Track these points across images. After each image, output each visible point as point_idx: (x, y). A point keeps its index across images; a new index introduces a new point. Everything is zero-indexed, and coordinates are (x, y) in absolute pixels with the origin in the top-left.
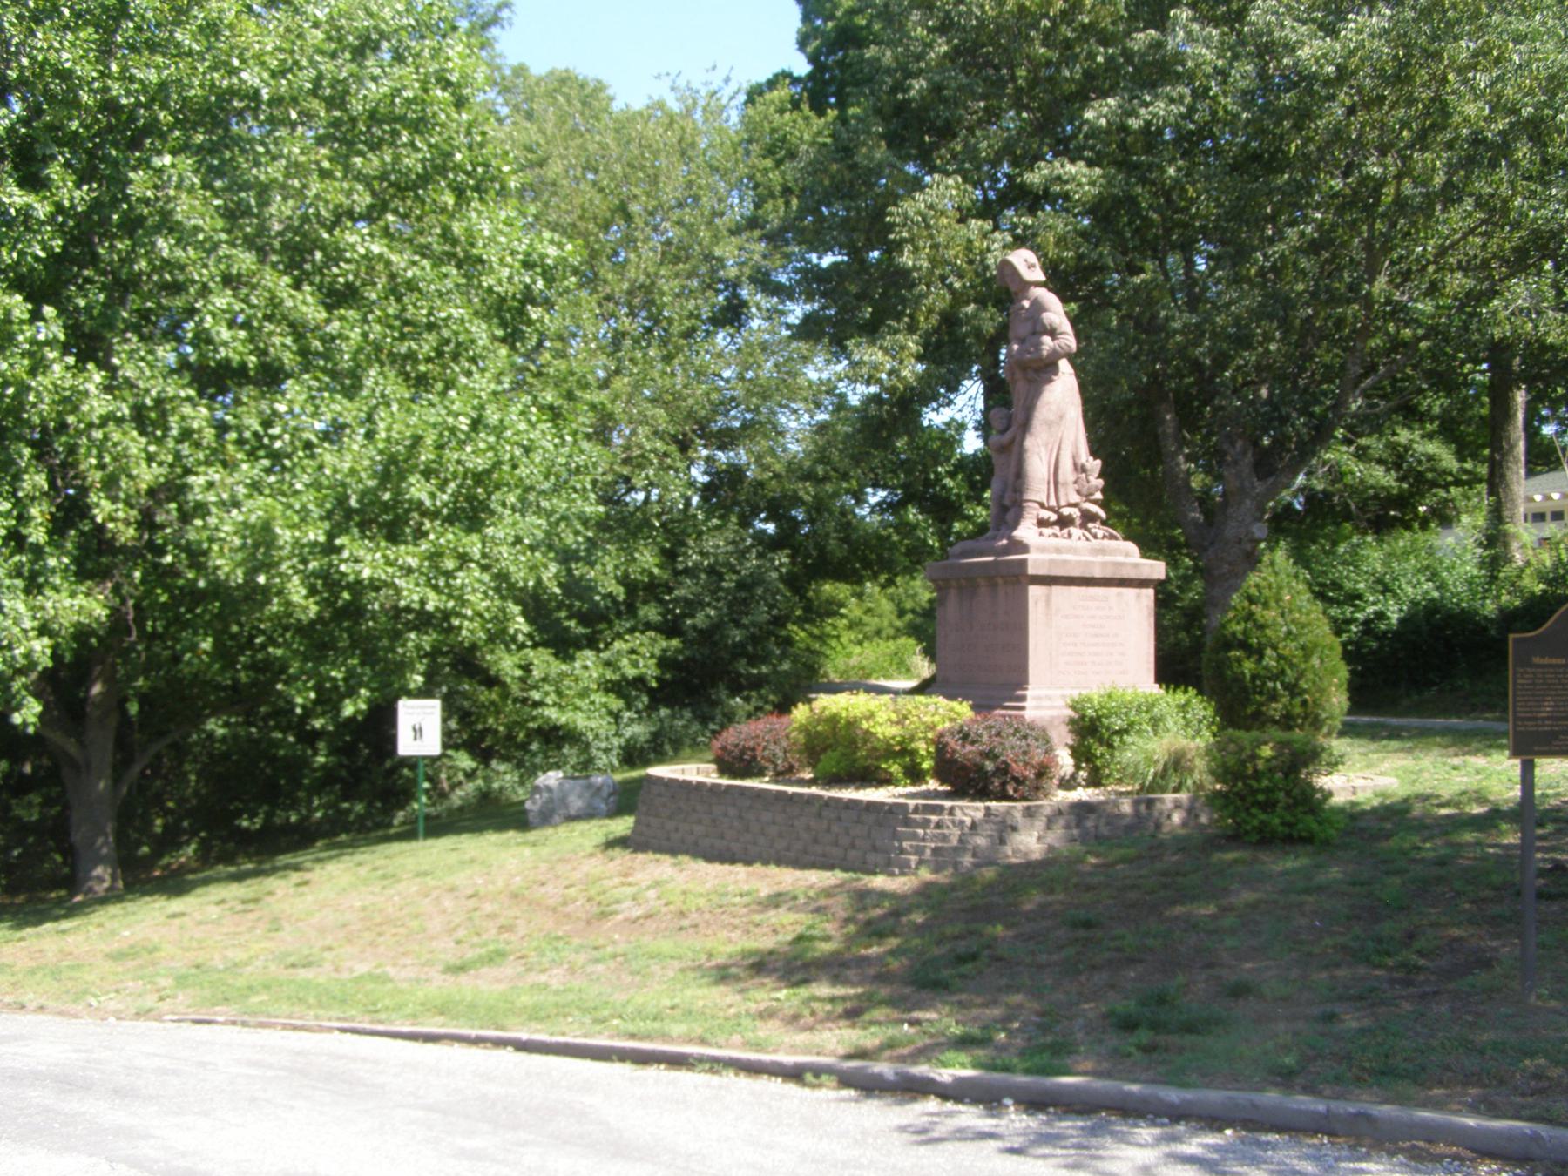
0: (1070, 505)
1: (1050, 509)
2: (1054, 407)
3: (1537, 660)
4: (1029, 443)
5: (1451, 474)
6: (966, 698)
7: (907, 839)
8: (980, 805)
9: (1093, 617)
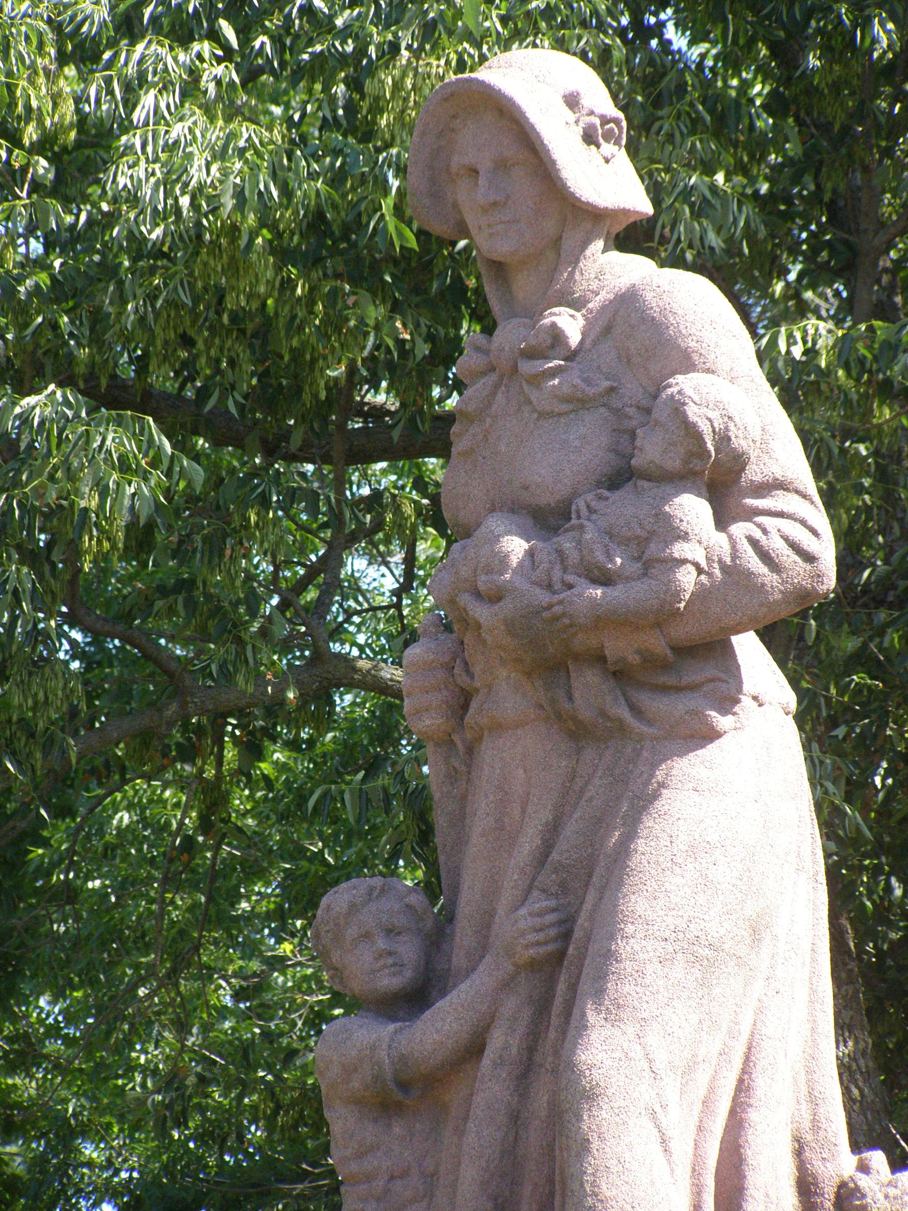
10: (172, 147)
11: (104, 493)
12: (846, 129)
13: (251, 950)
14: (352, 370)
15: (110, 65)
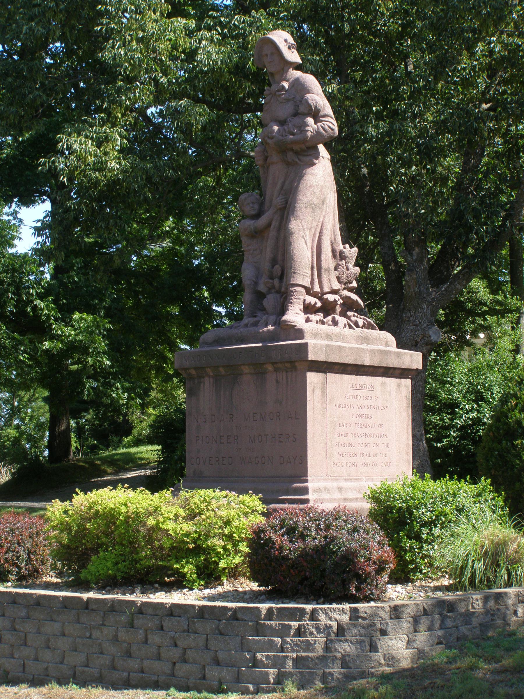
1: (314, 295)
4: (294, 225)
5: (485, 304)
6: (256, 492)
7: (262, 650)
8: (347, 606)
9: (361, 407)
10: (208, 52)
11: (196, 119)
12: (339, 47)
13: (227, 209)
14: (244, 95)
15: (196, 36)
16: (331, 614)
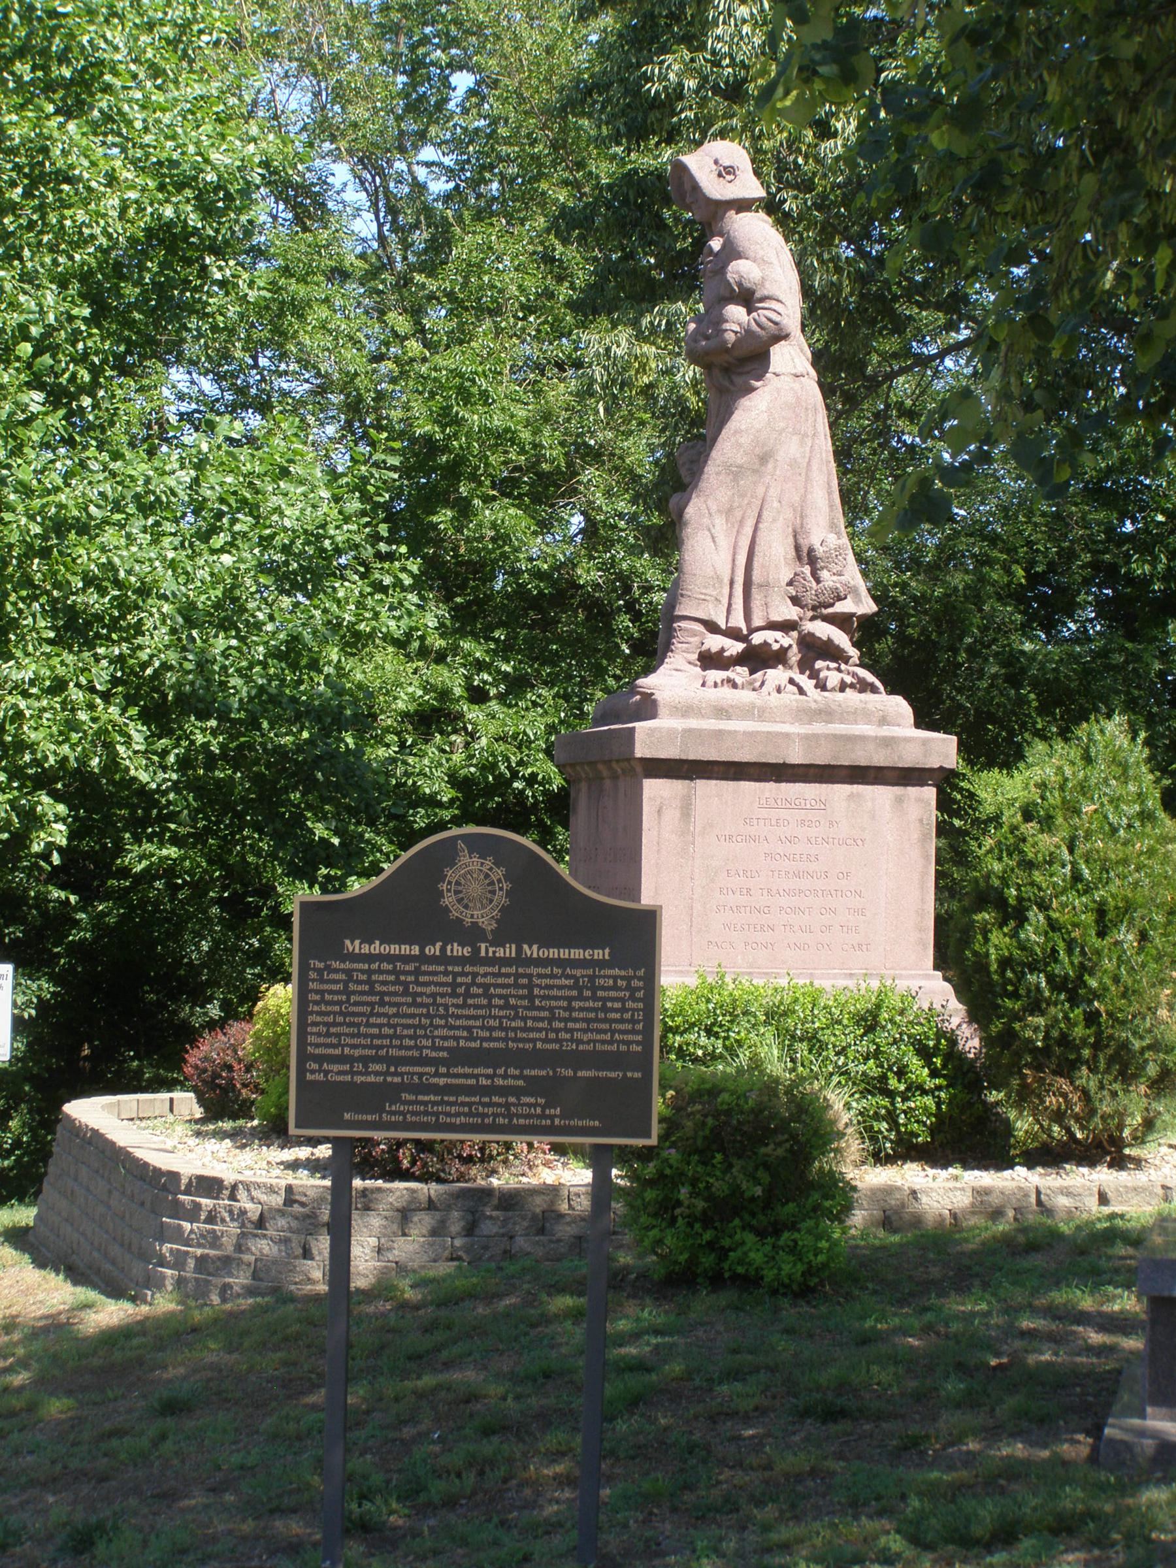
0: (772, 626)
1: (733, 634)
2: (744, 440)
3: (354, 946)
16: (254, 1193)
